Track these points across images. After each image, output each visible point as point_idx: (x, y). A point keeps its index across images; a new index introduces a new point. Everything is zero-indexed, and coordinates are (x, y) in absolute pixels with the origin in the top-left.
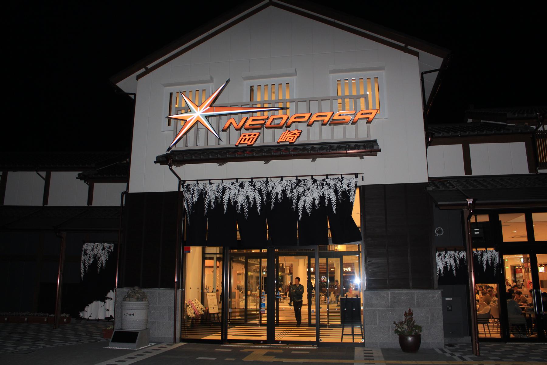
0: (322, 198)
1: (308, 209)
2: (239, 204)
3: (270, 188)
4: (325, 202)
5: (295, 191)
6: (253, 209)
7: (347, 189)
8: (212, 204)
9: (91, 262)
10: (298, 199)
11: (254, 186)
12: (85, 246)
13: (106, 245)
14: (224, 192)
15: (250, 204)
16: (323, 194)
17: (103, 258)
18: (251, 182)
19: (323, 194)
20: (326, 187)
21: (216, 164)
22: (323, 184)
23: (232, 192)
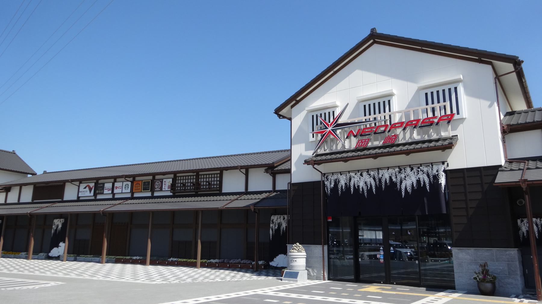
0: (418, 181)
1: (409, 189)
2: (361, 188)
3: (380, 176)
4: (421, 184)
5: (398, 177)
6: (370, 190)
7: (437, 173)
8: (343, 188)
9: (276, 228)
10: (401, 182)
11: (370, 175)
12: (272, 217)
13: (286, 217)
14: (350, 180)
15: (367, 187)
16: (419, 178)
17: (284, 225)
18: (368, 172)
19: (419, 178)
20: (421, 173)
21: (440, 151)
22: (418, 171)
23: (356, 180)
